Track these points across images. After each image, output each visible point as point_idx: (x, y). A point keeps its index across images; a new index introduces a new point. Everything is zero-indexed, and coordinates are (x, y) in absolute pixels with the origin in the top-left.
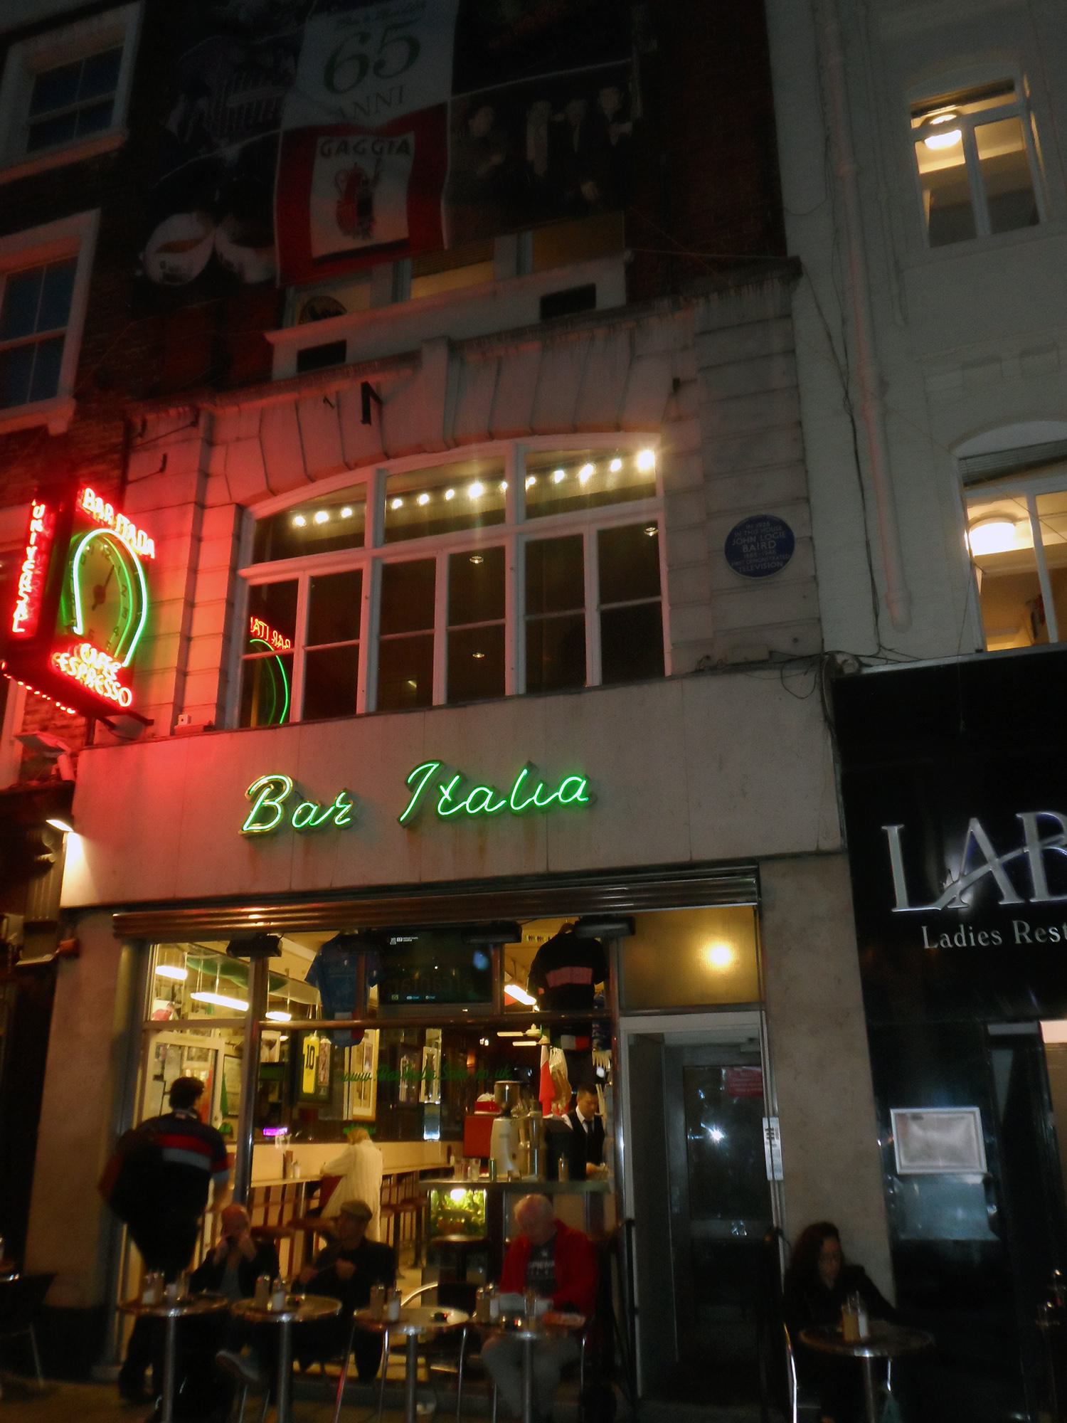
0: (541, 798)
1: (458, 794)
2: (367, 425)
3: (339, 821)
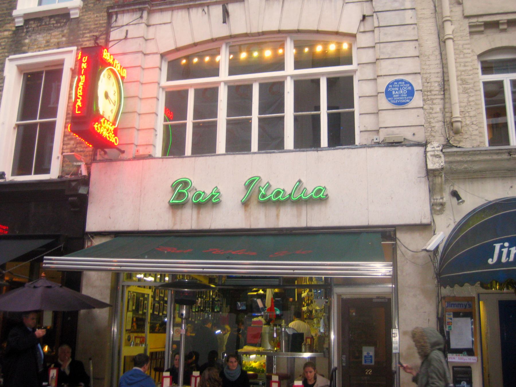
2: (225, 24)
3: (214, 200)
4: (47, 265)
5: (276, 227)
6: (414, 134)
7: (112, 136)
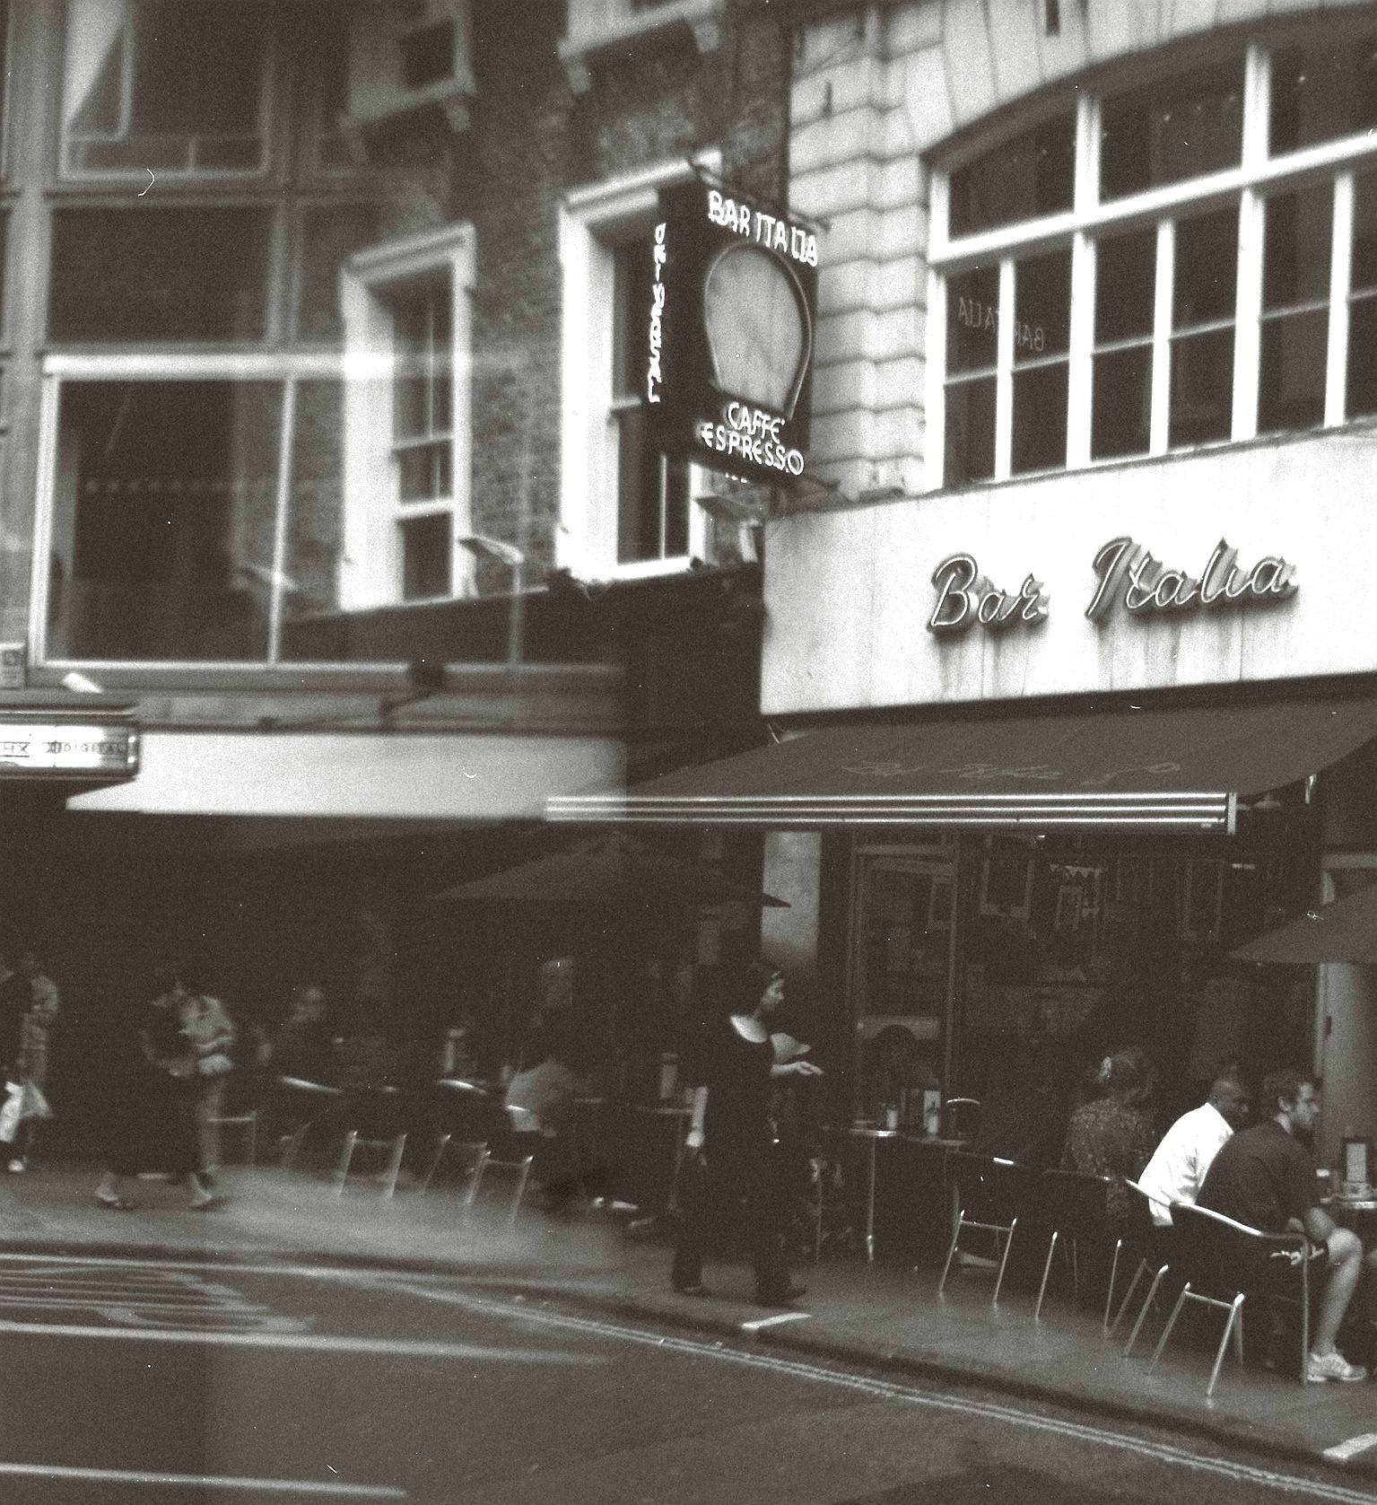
5: (1170, 684)
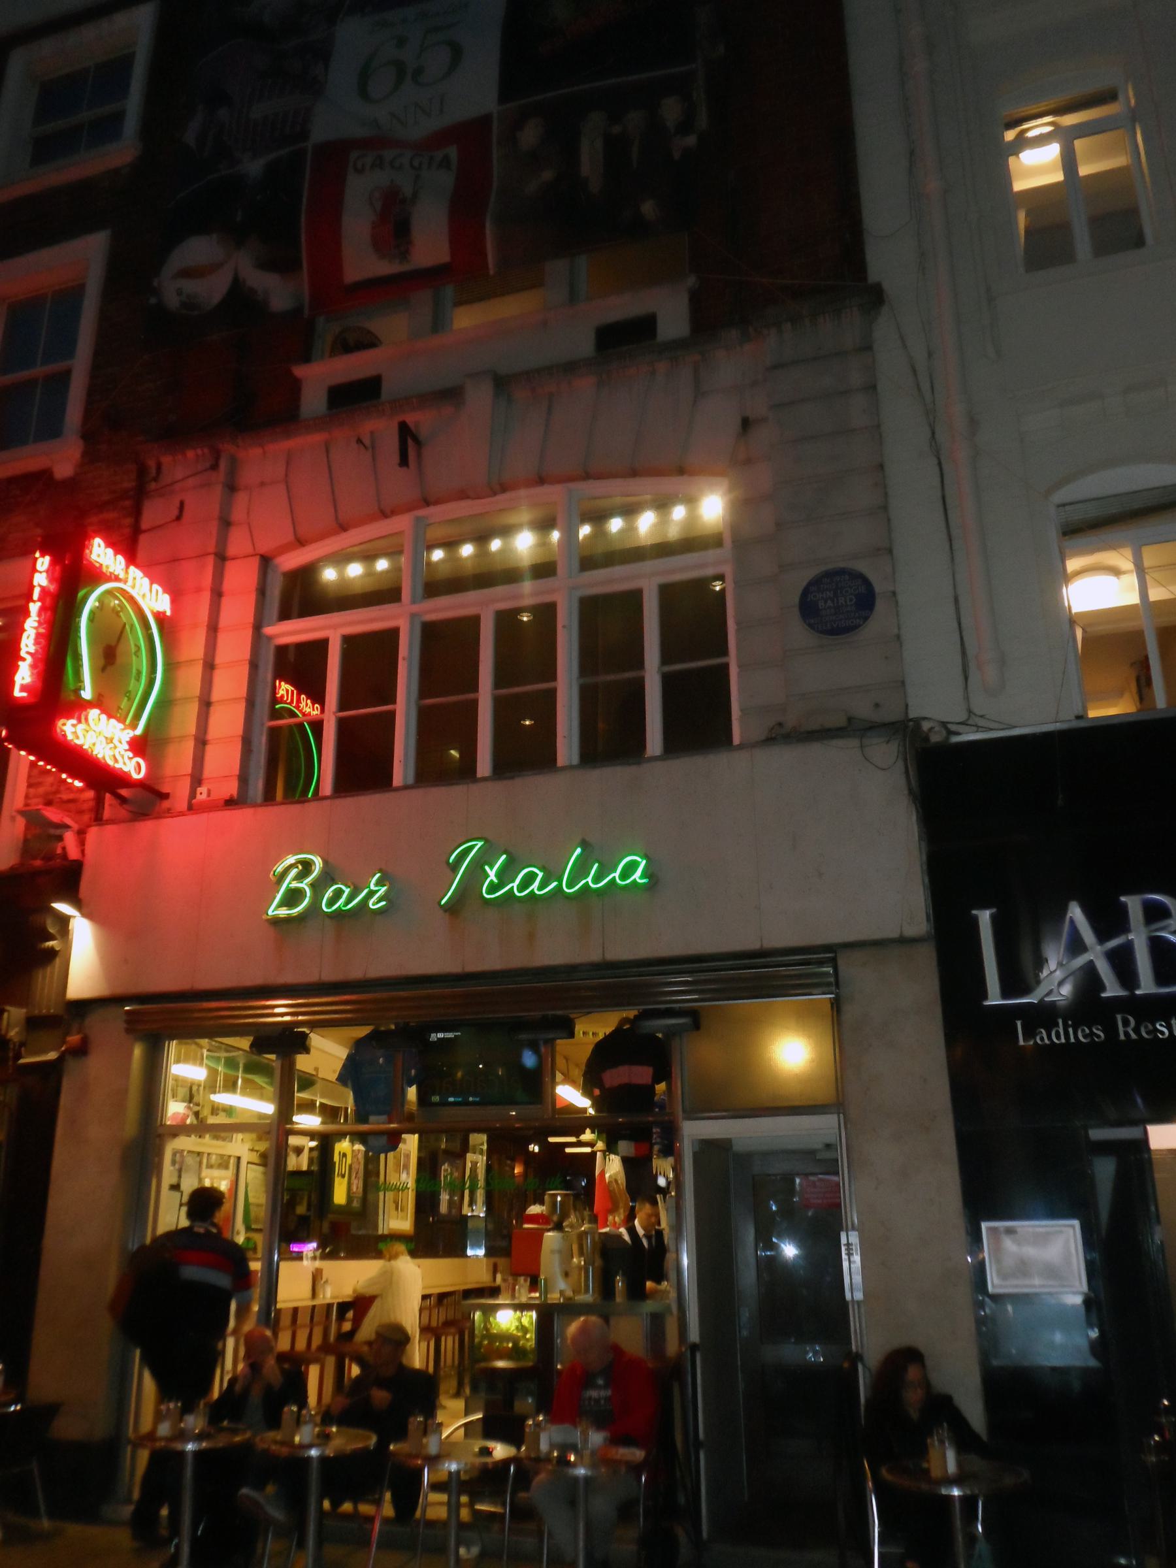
0: (597, 879)
1: (505, 875)
2: (405, 469)
4: (166, 1045)
6: (877, 705)
7: (122, 756)
